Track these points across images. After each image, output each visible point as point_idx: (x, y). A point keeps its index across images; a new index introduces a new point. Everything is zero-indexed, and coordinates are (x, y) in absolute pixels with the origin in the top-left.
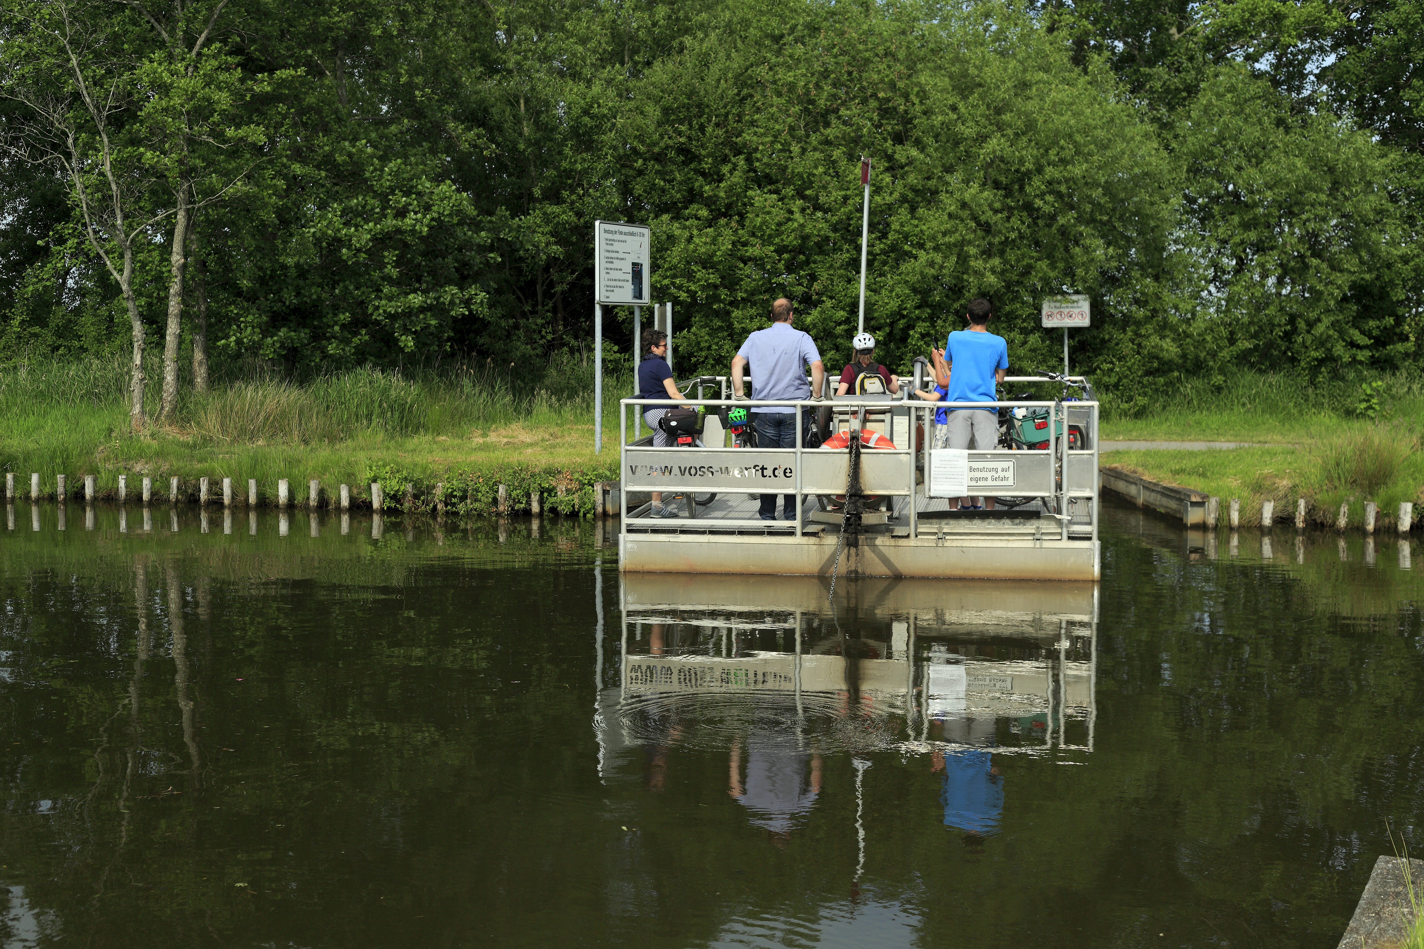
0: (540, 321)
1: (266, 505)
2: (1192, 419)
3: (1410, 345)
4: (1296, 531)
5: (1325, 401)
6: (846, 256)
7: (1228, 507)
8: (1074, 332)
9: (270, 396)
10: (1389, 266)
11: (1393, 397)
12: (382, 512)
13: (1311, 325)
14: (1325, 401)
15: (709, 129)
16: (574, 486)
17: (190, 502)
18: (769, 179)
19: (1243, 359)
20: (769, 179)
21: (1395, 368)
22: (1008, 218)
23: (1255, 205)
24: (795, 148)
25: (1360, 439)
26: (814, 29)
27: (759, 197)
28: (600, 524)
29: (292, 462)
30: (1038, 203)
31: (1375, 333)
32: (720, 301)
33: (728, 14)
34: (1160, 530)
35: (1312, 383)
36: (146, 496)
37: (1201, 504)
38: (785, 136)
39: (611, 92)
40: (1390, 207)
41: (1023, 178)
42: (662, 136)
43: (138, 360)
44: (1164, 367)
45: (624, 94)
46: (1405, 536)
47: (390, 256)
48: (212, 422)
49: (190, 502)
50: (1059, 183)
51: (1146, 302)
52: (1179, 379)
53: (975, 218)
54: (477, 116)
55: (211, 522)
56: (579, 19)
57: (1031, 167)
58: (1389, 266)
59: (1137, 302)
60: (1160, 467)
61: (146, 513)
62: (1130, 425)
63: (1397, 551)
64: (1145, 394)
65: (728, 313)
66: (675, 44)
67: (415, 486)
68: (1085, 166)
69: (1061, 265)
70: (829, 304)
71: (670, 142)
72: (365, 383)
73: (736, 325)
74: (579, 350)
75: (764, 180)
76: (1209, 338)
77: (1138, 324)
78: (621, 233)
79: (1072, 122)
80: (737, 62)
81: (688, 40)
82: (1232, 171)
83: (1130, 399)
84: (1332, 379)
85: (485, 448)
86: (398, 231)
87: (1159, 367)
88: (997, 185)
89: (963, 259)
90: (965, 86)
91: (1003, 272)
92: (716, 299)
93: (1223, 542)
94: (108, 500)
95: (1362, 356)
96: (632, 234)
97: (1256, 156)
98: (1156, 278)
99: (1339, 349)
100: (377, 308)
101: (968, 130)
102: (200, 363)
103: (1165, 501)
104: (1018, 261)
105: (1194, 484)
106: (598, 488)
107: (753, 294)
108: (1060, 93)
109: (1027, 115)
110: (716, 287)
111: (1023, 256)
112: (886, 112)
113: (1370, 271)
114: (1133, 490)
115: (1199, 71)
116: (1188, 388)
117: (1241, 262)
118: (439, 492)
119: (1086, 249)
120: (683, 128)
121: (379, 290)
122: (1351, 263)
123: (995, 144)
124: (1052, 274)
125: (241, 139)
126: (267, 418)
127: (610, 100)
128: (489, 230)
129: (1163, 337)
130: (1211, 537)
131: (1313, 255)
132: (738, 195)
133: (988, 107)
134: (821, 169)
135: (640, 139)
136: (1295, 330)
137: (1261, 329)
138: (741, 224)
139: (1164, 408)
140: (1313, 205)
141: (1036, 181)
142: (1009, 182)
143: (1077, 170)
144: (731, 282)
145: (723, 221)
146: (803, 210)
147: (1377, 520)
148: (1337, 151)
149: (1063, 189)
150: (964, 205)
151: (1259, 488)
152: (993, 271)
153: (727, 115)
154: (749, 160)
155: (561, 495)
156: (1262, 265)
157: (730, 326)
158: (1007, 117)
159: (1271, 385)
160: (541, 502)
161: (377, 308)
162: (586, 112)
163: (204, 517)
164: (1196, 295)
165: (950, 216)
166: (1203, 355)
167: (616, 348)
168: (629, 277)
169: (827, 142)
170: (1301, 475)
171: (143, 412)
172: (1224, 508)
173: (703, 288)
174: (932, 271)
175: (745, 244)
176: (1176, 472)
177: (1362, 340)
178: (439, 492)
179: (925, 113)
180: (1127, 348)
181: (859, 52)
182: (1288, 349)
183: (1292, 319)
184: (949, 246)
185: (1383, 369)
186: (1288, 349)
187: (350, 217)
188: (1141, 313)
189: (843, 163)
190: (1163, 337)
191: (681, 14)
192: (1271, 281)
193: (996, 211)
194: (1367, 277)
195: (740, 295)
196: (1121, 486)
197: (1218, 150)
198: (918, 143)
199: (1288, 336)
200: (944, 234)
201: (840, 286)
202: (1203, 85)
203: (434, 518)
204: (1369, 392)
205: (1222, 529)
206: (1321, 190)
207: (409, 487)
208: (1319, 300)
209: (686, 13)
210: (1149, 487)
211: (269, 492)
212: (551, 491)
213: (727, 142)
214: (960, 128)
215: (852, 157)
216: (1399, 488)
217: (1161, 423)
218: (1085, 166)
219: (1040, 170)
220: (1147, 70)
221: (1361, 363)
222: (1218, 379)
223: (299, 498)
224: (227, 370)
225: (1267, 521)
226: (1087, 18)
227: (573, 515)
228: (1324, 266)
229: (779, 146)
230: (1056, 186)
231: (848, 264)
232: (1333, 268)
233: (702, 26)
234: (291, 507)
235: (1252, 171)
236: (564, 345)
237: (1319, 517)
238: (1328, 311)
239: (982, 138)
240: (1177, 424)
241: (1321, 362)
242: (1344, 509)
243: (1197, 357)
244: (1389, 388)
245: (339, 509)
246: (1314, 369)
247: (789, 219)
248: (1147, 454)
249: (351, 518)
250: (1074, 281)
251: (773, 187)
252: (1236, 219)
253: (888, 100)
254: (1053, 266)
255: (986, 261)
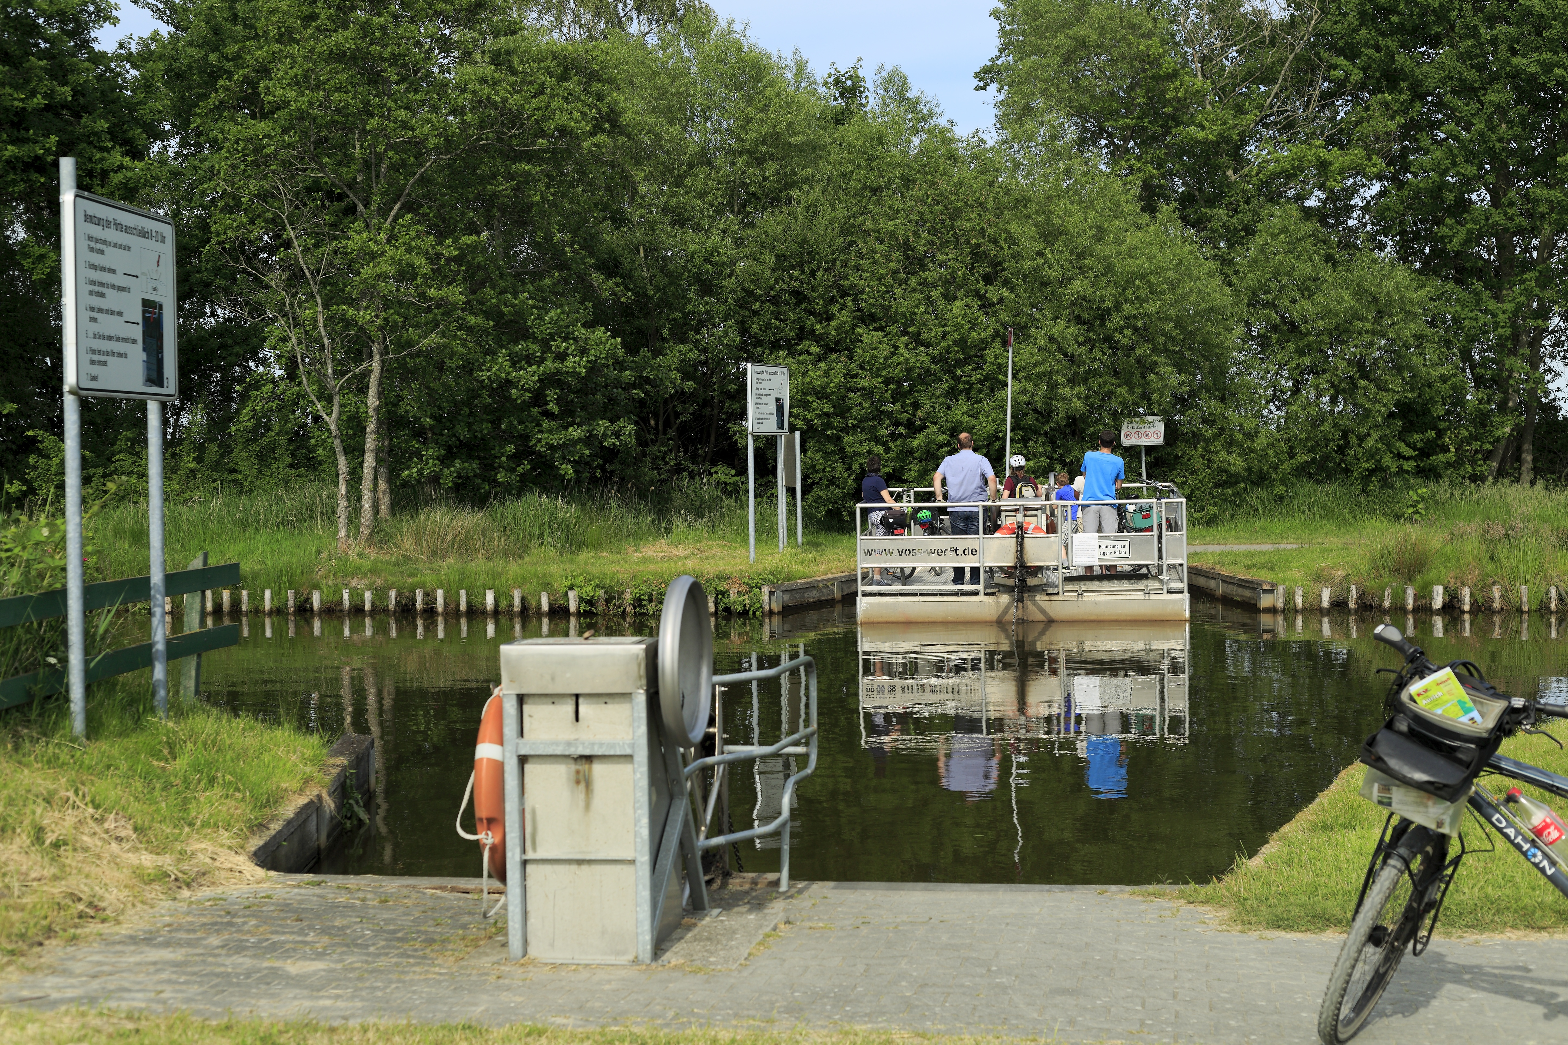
0: (662, 449)
1: (475, 613)
2: (1258, 525)
3: (1451, 456)
4: (1349, 611)
5: (1377, 507)
6: (945, 385)
7: (1293, 594)
8: (1150, 449)
9: (445, 520)
10: (1430, 385)
11: (1437, 503)
12: (579, 614)
13: (1361, 439)
14: (1377, 507)
15: (820, 274)
16: (743, 588)
17: (406, 611)
18: (873, 318)
19: (1301, 471)
20: (873, 318)
21: (1438, 476)
22: (1091, 350)
23: (1308, 333)
24: (898, 291)
25: (1400, 536)
26: (908, 181)
27: (869, 336)
28: (767, 620)
29: (496, 575)
30: (1118, 336)
31: (1419, 445)
32: (833, 428)
33: (829, 168)
34: (1238, 616)
35: (1364, 491)
36: (368, 607)
37: (1271, 591)
38: (888, 279)
39: (727, 241)
40: (1429, 331)
41: (1103, 315)
42: (777, 281)
43: (343, 490)
44: (1233, 480)
45: (739, 243)
46: (1438, 612)
47: (552, 394)
48: (408, 543)
49: (406, 611)
50: (1135, 317)
51: (1214, 421)
52: (1245, 490)
53: (1060, 350)
54: (611, 267)
55: (426, 628)
56: (696, 176)
57: (1111, 305)
58: (1430, 385)
59: (1205, 421)
60: (1235, 563)
61: (368, 621)
62: (1203, 532)
63: (1432, 626)
64: (1215, 504)
65: (839, 439)
66: (783, 196)
67: (606, 592)
68: (1158, 303)
69: (1139, 390)
70: (933, 428)
71: (785, 286)
72: (535, 506)
73: (848, 449)
74: (700, 474)
75: (868, 319)
76: (1271, 453)
77: (1208, 441)
78: (119, 227)
79: (1147, 265)
80: (841, 213)
81: (795, 193)
82: (1287, 303)
83: (1202, 509)
84: (1381, 487)
85: (645, 560)
86: (559, 372)
87: (1227, 480)
88: (1079, 320)
89: (1053, 387)
90: (1050, 235)
91: (1087, 397)
92: (829, 426)
93: (1290, 625)
94: (331, 611)
95: (1408, 466)
96: (775, 373)
97: (1308, 289)
98: (1223, 399)
99: (1387, 460)
100: (539, 441)
101: (1054, 274)
102: (384, 492)
103: (1240, 591)
104: (1100, 387)
105: (1264, 576)
106: (765, 590)
107: (861, 421)
108: (1134, 238)
109: (1105, 258)
110: (827, 415)
111: (1105, 383)
112: (977, 255)
113: (1412, 390)
114: (1212, 584)
115: (1255, 213)
116: (1255, 497)
117: (1296, 383)
118: (628, 596)
119: (1161, 377)
120: (796, 273)
121: (539, 425)
122: (1395, 383)
123: (1079, 286)
124: (1131, 399)
125: (442, 299)
126: (454, 539)
127: (728, 249)
128: (632, 369)
129: (1230, 453)
130: (1280, 619)
131: (1361, 377)
132: (846, 332)
133: (1072, 254)
134: (922, 309)
135: (756, 283)
136: (1347, 444)
137: (1318, 444)
138: (850, 358)
139: (1233, 516)
140: (1360, 333)
141: (1116, 317)
142: (1092, 318)
143: (1152, 307)
144: (842, 411)
145: (833, 356)
146: (907, 345)
147: (1415, 601)
148: (1379, 286)
149: (1140, 323)
150: (1051, 339)
151: (1318, 578)
152: (1079, 398)
153: (835, 260)
154: (855, 301)
155: (733, 597)
156: (1317, 387)
157: (842, 449)
158: (1088, 262)
159: (1327, 494)
160: (716, 603)
161: (539, 441)
162: (707, 260)
163: (419, 623)
164: (1259, 415)
165: (1040, 349)
166: (1266, 468)
167: (733, 472)
168: (774, 410)
169: (924, 283)
170: (1353, 566)
171: (348, 535)
172: (1290, 594)
173: (819, 416)
174: (1025, 398)
175: (856, 376)
176: (1249, 567)
177: (1409, 452)
178: (628, 596)
179: (1013, 257)
180: (1198, 463)
181: (952, 202)
182: (1342, 461)
183: (1345, 435)
184: (1039, 376)
185: (1428, 478)
186: (1342, 461)
187: (515, 362)
188: (1209, 433)
189: (942, 303)
190: (1230, 453)
191: (788, 170)
192: (1326, 399)
193: (1080, 344)
194: (1410, 395)
195: (851, 422)
196: (1201, 581)
197: (1275, 285)
198: (1006, 283)
199: (1341, 450)
200: (1035, 365)
201: (941, 412)
202: (1260, 226)
203: (624, 618)
204: (1415, 498)
205: (1289, 611)
206: (1367, 319)
207: (601, 593)
208: (1368, 416)
209: (793, 169)
210: (1226, 580)
211: (477, 601)
212: (725, 593)
213: (836, 285)
214: (1047, 271)
215: (949, 297)
216: (1433, 575)
217: (1230, 530)
218: (1158, 303)
219: (1117, 307)
220: (1208, 211)
221: (1408, 472)
222: (1280, 489)
223: (503, 605)
224: (407, 498)
225: (1325, 604)
226: (1152, 163)
227: (744, 614)
228: (1371, 386)
229: (883, 289)
230: (1133, 321)
231: (948, 392)
232: (1380, 388)
233: (807, 180)
234: (496, 613)
235: (1306, 303)
236: (684, 470)
237: (1368, 600)
238: (1376, 426)
239: (1065, 281)
240: (1244, 530)
241: (1372, 472)
242: (1388, 592)
243: (1261, 470)
244: (1434, 494)
245: (539, 614)
246: (1366, 478)
247: (894, 354)
248: (1221, 554)
249: (550, 621)
250: (1150, 405)
251: (877, 325)
252: (1292, 346)
253: (979, 245)
254: (1131, 391)
255: (1072, 388)
